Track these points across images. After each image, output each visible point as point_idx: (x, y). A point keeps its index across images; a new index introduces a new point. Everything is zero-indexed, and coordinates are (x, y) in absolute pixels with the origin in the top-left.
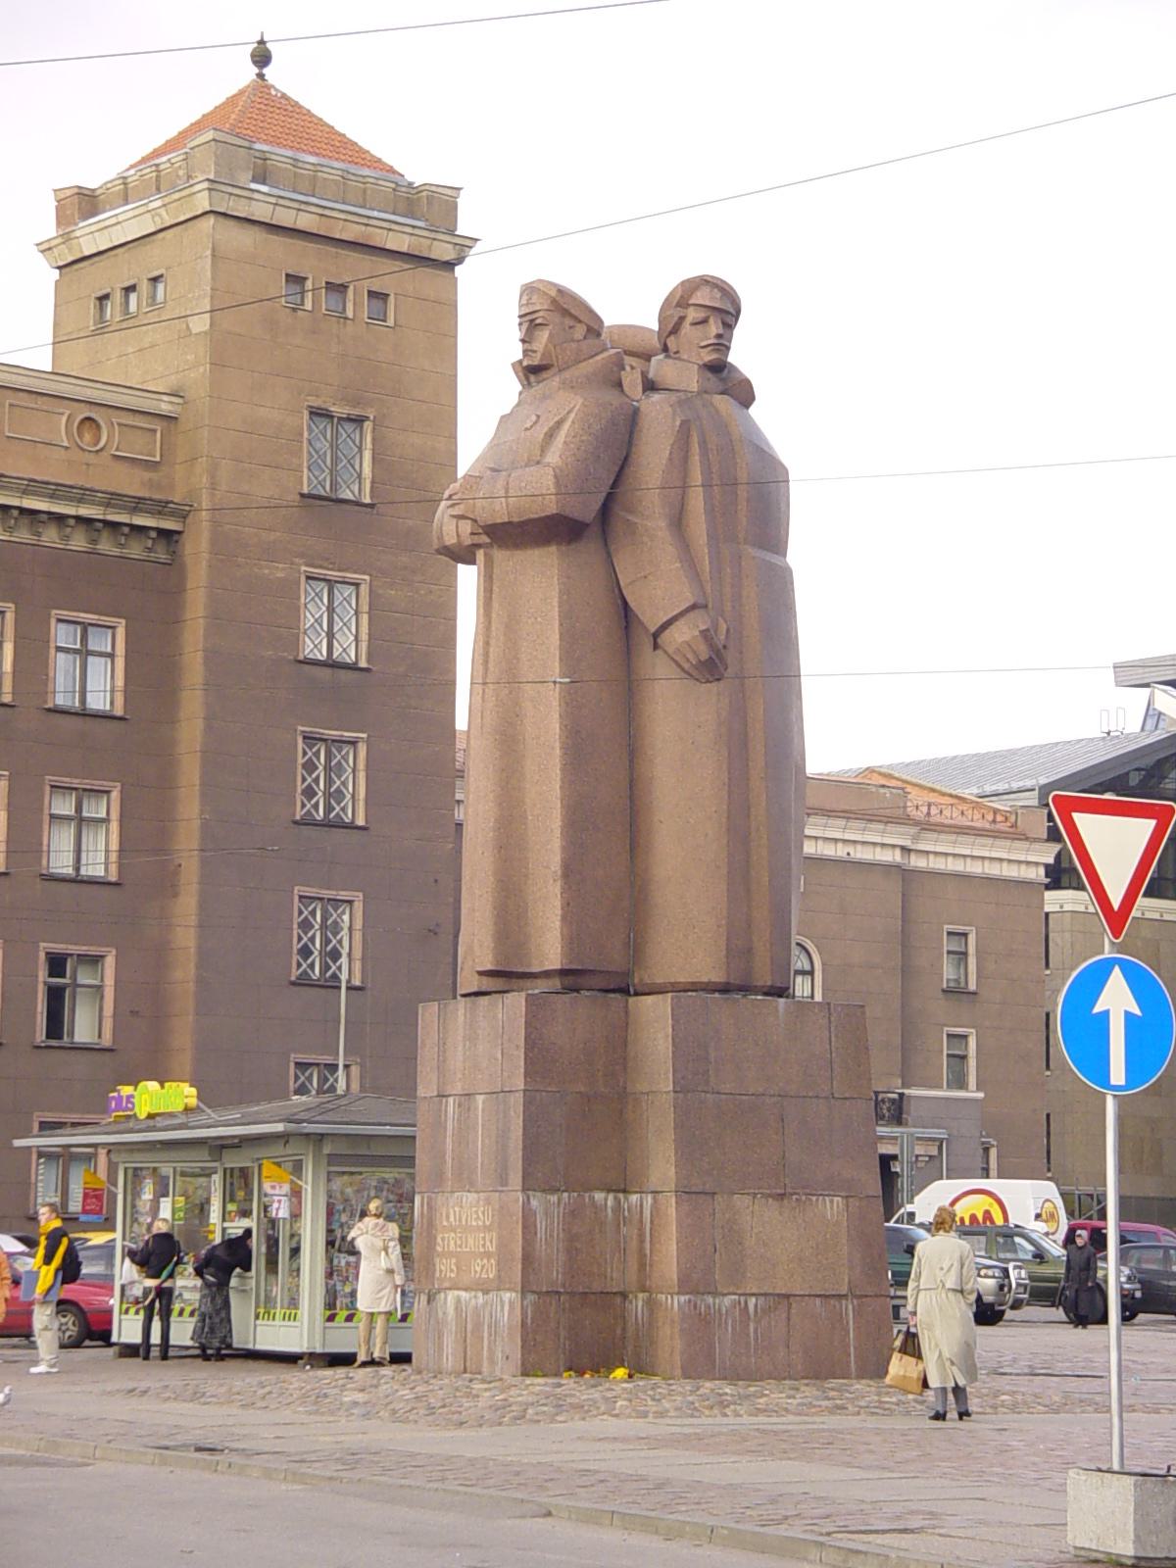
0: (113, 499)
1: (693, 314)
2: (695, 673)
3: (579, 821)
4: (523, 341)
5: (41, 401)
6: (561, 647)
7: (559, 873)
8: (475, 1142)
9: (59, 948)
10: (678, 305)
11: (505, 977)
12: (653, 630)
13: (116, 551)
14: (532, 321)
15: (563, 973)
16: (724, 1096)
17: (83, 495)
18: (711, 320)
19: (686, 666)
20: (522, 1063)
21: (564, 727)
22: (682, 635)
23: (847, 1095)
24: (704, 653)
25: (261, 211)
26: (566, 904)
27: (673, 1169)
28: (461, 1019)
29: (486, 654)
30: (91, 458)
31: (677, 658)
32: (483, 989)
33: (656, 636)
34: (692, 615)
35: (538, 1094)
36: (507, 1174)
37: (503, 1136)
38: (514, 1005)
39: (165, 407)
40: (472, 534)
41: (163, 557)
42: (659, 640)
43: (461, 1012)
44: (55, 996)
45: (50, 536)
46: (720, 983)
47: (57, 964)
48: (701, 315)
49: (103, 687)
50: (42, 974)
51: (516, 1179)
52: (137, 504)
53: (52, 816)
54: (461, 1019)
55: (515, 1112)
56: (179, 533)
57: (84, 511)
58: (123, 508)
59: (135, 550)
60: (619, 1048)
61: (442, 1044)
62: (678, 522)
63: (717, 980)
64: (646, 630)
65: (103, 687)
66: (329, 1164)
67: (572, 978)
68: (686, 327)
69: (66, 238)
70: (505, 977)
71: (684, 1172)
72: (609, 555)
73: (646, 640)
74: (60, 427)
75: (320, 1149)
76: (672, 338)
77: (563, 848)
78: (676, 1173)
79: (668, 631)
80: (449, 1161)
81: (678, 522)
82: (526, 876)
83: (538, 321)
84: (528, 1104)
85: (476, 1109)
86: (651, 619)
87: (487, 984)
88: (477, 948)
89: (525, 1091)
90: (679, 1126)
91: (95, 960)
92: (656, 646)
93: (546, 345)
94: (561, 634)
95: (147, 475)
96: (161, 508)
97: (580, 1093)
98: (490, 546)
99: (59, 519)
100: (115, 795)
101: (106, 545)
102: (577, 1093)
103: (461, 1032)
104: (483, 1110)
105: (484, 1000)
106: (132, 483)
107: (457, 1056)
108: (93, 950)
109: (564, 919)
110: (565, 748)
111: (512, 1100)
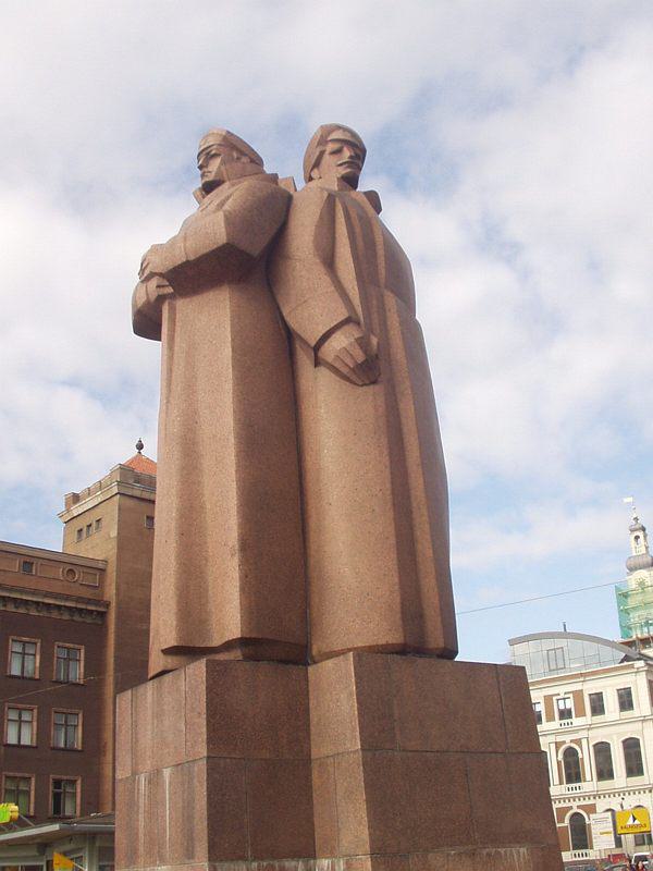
0: (79, 599)
1: (330, 147)
2: (354, 378)
3: (253, 547)
4: (201, 167)
5: (51, 563)
6: (234, 358)
7: (237, 547)
8: (163, 817)
9: (58, 777)
10: (319, 144)
11: (184, 652)
12: (313, 343)
13: (80, 620)
14: (208, 154)
15: (242, 642)
16: (409, 754)
17: (67, 598)
18: (345, 149)
19: (345, 370)
20: (205, 729)
21: (237, 421)
22: (340, 342)
23: (520, 749)
24: (360, 357)
25: (137, 493)
26: (245, 578)
27: (367, 832)
28: (149, 699)
29: (170, 371)
30: (72, 585)
31: (337, 365)
32: (169, 667)
33: (317, 348)
34: (346, 327)
35: (222, 762)
36: (193, 847)
37: (189, 805)
38: (199, 668)
39: (100, 566)
40: (158, 287)
41: (100, 622)
42: (320, 354)
43: (149, 693)
44: (57, 797)
45: (55, 614)
46: (398, 645)
47: (57, 784)
48: (336, 146)
49: (78, 672)
50: (51, 788)
51: (202, 849)
52: (89, 601)
53: (55, 724)
54: (149, 699)
55: (200, 782)
56: (105, 613)
57: (68, 604)
58: (83, 602)
59: (89, 620)
60: (296, 716)
61: (135, 725)
62: (329, 262)
63: (394, 642)
64: (305, 342)
65: (78, 672)
66: (100, 860)
67: (251, 646)
68: (327, 158)
69: (68, 510)
70: (184, 652)
71: (378, 832)
72: (272, 292)
73: (308, 362)
74: (60, 572)
75: (94, 843)
76: (316, 170)
77: (240, 526)
78: (370, 834)
79: (326, 344)
80: (141, 835)
81: (329, 262)
82: (206, 560)
83: (213, 152)
84: (211, 770)
85: (164, 782)
86: (312, 334)
87: (170, 661)
88: (164, 628)
89: (208, 757)
90: (371, 786)
91: (73, 782)
92: (317, 362)
93: (219, 167)
94: (233, 348)
95: (93, 591)
96: (98, 602)
97: (265, 760)
98: (172, 297)
99: (59, 607)
100: (80, 715)
101: (77, 618)
102: (261, 759)
103: (149, 712)
104: (170, 783)
105: (167, 678)
106: (87, 593)
107: (147, 738)
108: (72, 778)
109: (242, 589)
110: (238, 436)
111: (196, 769)
